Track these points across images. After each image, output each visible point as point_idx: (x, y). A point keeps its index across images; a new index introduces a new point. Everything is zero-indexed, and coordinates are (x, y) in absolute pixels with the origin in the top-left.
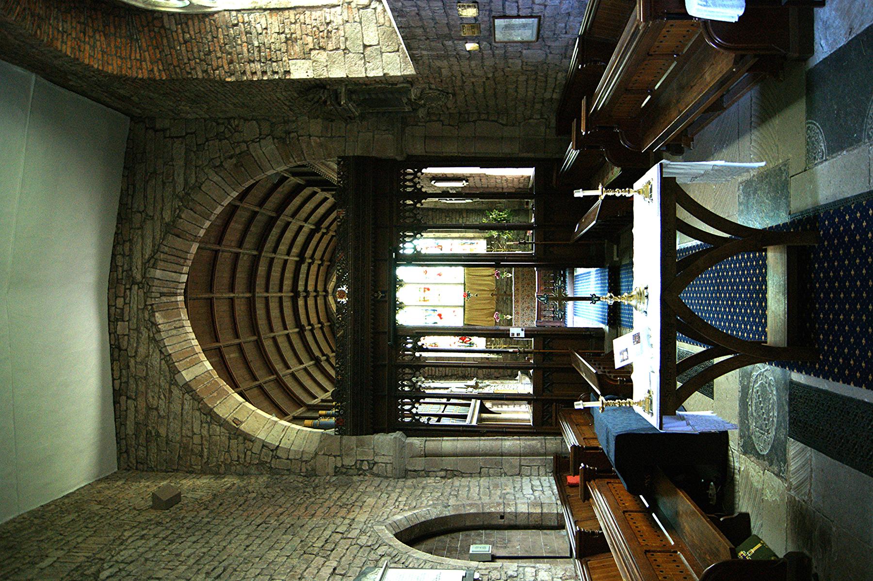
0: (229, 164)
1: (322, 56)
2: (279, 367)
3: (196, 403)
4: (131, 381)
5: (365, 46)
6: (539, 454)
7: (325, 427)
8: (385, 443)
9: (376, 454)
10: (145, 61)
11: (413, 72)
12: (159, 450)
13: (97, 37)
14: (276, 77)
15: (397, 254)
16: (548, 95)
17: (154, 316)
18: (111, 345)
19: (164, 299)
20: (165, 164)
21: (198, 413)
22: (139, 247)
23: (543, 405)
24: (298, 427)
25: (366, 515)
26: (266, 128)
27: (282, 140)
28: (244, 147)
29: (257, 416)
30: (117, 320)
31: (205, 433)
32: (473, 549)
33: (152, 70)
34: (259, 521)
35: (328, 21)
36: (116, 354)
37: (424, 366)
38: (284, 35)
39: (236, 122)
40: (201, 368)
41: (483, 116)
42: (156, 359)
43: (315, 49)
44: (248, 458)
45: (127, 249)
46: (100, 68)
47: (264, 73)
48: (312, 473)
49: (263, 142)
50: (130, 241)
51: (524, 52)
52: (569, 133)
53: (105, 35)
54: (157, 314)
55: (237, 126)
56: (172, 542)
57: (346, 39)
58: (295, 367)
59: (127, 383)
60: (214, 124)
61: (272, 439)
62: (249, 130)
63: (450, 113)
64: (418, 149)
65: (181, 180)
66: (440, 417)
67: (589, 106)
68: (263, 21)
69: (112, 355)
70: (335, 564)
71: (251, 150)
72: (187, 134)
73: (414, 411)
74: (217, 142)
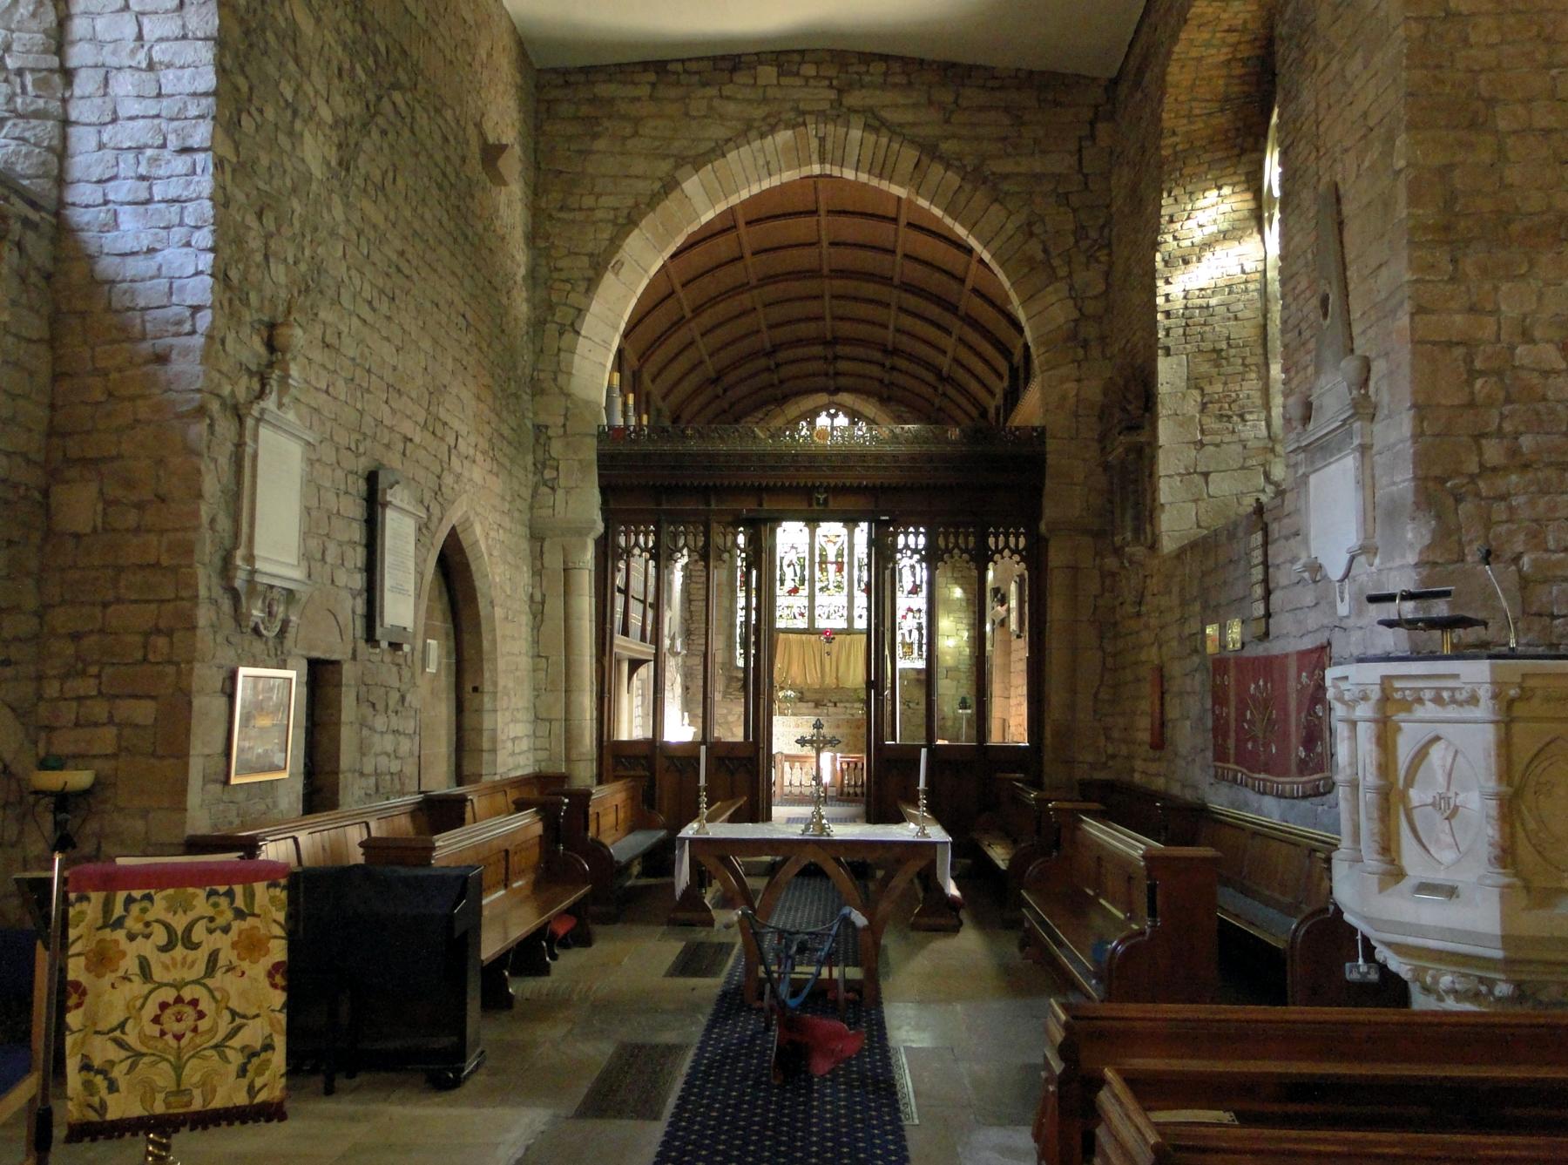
0: (1034, 248)
1: (1191, 406)
2: (706, 319)
3: (647, 200)
4: (680, 91)
5: (1206, 475)
6: (568, 749)
7: (609, 408)
8: (585, 504)
9: (568, 491)
10: (1190, 123)
11: (1166, 551)
12: (569, 139)
13: (1224, 50)
14: (1161, 334)
15: (888, 524)
16: (1138, 764)
17: (786, 128)
18: (739, 56)
19: (814, 144)
20: (1036, 141)
21: (630, 202)
22: (901, 101)
23: (646, 757)
24: (609, 365)
25: (480, 481)
26: (1091, 307)
27: (1073, 336)
28: (1062, 272)
29: (626, 298)
30: (779, 66)
31: (599, 214)
32: (432, 643)
33: (1174, 133)
34: (469, 315)
35: (1248, 417)
36: (722, 65)
37: (707, 567)
38: (1224, 346)
39: (1103, 259)
40: (703, 201)
41: (1109, 660)
42: (718, 132)
43: (1203, 395)
44: (561, 285)
45: (897, 79)
46: (1175, 57)
47: (1168, 314)
48: (538, 390)
49: (1071, 303)
50: (910, 84)
51: (1188, 723)
52: (1085, 799)
53: (1229, 61)
54: (790, 133)
55: (1097, 261)
56: (440, 188)
57: (1217, 445)
58: (703, 347)
59: (678, 83)
60: (1101, 221)
61: (589, 325)
62: (1090, 278)
63: (1114, 608)
64: (1057, 557)
65: (1007, 166)
66: (625, 591)
67: (1088, 813)
68: (1248, 314)
69: (723, 58)
70: (417, 440)
71: (1058, 284)
72: (1086, 176)
73: (637, 551)
74: (1071, 227)
